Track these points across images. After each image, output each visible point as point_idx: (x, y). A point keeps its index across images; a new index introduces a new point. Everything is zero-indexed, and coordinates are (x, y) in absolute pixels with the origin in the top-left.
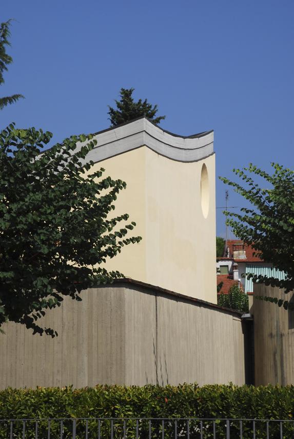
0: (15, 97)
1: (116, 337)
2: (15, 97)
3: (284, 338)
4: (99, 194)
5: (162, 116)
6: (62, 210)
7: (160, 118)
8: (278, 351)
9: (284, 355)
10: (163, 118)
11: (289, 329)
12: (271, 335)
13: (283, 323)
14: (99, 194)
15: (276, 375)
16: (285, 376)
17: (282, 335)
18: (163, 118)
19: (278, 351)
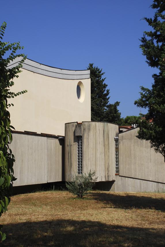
0: (106, 78)
1: (152, 212)
2: (106, 78)
3: (72, 146)
4: (19, 64)
5: (104, 72)
6: (2, 151)
7: (103, 73)
8: (70, 152)
9: (72, 154)
10: (104, 73)
11: (74, 142)
12: (68, 145)
13: (72, 140)
14: (19, 64)
15: (69, 162)
16: (72, 162)
17: (71, 145)
18: (104, 73)
19: (70, 152)
